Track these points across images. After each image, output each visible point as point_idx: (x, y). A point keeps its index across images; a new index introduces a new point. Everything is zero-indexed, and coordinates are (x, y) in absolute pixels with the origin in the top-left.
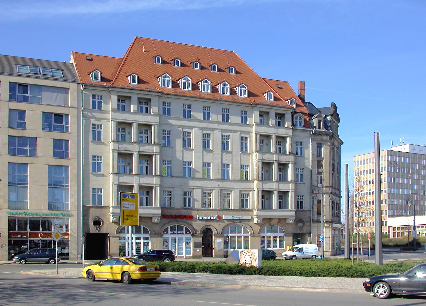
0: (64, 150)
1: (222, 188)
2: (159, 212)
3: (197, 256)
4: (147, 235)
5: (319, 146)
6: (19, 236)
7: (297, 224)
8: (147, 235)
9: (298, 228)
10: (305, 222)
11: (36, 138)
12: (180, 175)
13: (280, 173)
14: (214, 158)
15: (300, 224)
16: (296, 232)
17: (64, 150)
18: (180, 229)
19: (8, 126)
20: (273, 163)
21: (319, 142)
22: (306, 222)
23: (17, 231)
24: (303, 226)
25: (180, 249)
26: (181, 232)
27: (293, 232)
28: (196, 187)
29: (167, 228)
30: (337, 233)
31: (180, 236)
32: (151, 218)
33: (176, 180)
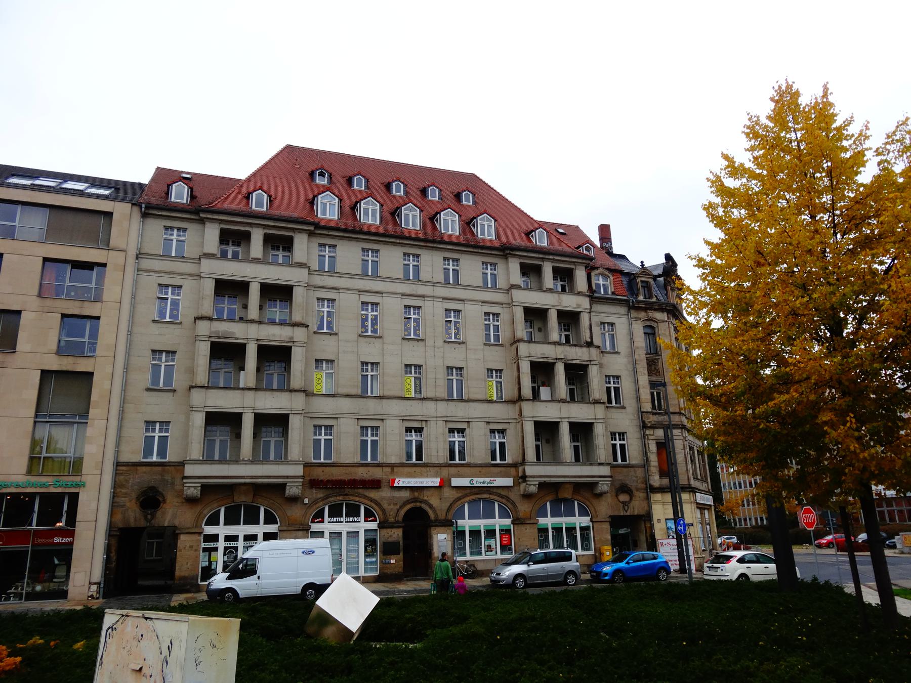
0: (86, 339)
1: (359, 414)
2: (299, 470)
3: (391, 574)
4: (272, 528)
5: (649, 331)
6: (57, 540)
7: (617, 496)
8: (272, 528)
9: (621, 505)
10: (634, 491)
11: (18, 313)
12: (359, 392)
13: (572, 387)
14: (392, 355)
15: (624, 497)
16: (616, 513)
17: (86, 339)
18: (353, 512)
19: (36, 292)
20: (554, 363)
21: (648, 323)
22: (637, 490)
23: (34, 526)
24: (631, 499)
25: (355, 560)
26: (339, 519)
27: (611, 513)
28: (389, 415)
29: (323, 510)
30: (707, 516)
31: (353, 527)
32: (283, 486)
33: (431, 405)
